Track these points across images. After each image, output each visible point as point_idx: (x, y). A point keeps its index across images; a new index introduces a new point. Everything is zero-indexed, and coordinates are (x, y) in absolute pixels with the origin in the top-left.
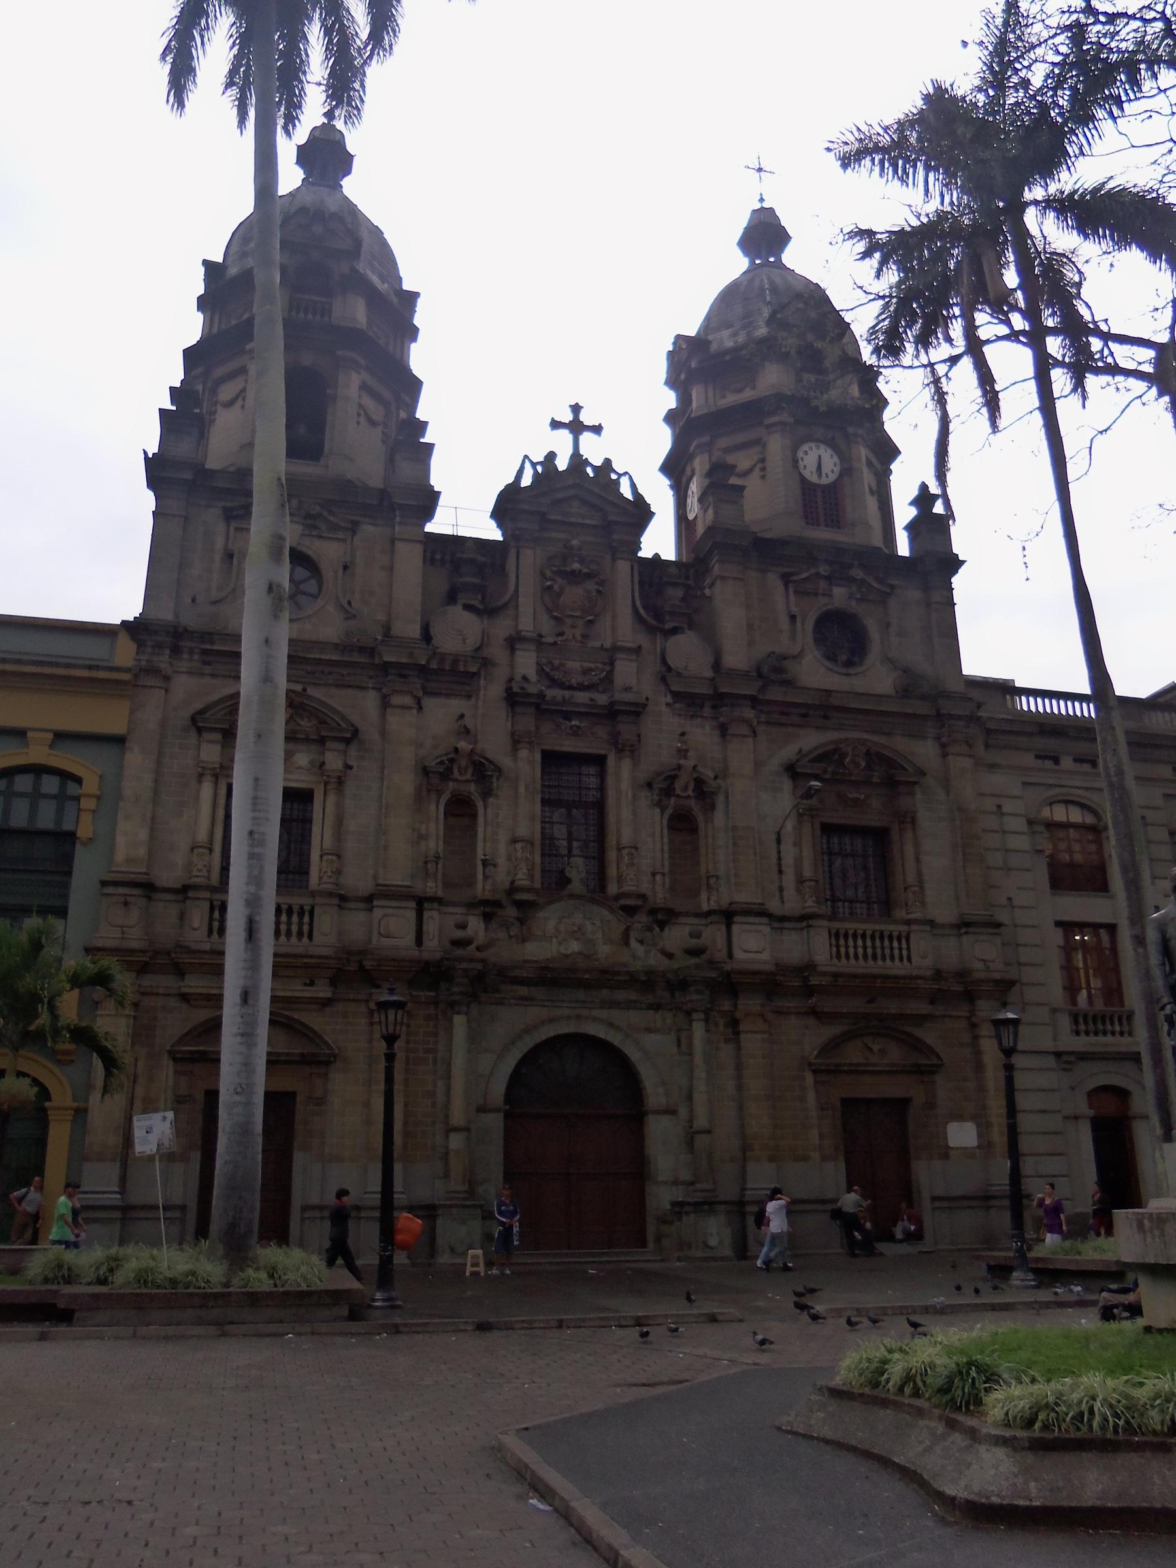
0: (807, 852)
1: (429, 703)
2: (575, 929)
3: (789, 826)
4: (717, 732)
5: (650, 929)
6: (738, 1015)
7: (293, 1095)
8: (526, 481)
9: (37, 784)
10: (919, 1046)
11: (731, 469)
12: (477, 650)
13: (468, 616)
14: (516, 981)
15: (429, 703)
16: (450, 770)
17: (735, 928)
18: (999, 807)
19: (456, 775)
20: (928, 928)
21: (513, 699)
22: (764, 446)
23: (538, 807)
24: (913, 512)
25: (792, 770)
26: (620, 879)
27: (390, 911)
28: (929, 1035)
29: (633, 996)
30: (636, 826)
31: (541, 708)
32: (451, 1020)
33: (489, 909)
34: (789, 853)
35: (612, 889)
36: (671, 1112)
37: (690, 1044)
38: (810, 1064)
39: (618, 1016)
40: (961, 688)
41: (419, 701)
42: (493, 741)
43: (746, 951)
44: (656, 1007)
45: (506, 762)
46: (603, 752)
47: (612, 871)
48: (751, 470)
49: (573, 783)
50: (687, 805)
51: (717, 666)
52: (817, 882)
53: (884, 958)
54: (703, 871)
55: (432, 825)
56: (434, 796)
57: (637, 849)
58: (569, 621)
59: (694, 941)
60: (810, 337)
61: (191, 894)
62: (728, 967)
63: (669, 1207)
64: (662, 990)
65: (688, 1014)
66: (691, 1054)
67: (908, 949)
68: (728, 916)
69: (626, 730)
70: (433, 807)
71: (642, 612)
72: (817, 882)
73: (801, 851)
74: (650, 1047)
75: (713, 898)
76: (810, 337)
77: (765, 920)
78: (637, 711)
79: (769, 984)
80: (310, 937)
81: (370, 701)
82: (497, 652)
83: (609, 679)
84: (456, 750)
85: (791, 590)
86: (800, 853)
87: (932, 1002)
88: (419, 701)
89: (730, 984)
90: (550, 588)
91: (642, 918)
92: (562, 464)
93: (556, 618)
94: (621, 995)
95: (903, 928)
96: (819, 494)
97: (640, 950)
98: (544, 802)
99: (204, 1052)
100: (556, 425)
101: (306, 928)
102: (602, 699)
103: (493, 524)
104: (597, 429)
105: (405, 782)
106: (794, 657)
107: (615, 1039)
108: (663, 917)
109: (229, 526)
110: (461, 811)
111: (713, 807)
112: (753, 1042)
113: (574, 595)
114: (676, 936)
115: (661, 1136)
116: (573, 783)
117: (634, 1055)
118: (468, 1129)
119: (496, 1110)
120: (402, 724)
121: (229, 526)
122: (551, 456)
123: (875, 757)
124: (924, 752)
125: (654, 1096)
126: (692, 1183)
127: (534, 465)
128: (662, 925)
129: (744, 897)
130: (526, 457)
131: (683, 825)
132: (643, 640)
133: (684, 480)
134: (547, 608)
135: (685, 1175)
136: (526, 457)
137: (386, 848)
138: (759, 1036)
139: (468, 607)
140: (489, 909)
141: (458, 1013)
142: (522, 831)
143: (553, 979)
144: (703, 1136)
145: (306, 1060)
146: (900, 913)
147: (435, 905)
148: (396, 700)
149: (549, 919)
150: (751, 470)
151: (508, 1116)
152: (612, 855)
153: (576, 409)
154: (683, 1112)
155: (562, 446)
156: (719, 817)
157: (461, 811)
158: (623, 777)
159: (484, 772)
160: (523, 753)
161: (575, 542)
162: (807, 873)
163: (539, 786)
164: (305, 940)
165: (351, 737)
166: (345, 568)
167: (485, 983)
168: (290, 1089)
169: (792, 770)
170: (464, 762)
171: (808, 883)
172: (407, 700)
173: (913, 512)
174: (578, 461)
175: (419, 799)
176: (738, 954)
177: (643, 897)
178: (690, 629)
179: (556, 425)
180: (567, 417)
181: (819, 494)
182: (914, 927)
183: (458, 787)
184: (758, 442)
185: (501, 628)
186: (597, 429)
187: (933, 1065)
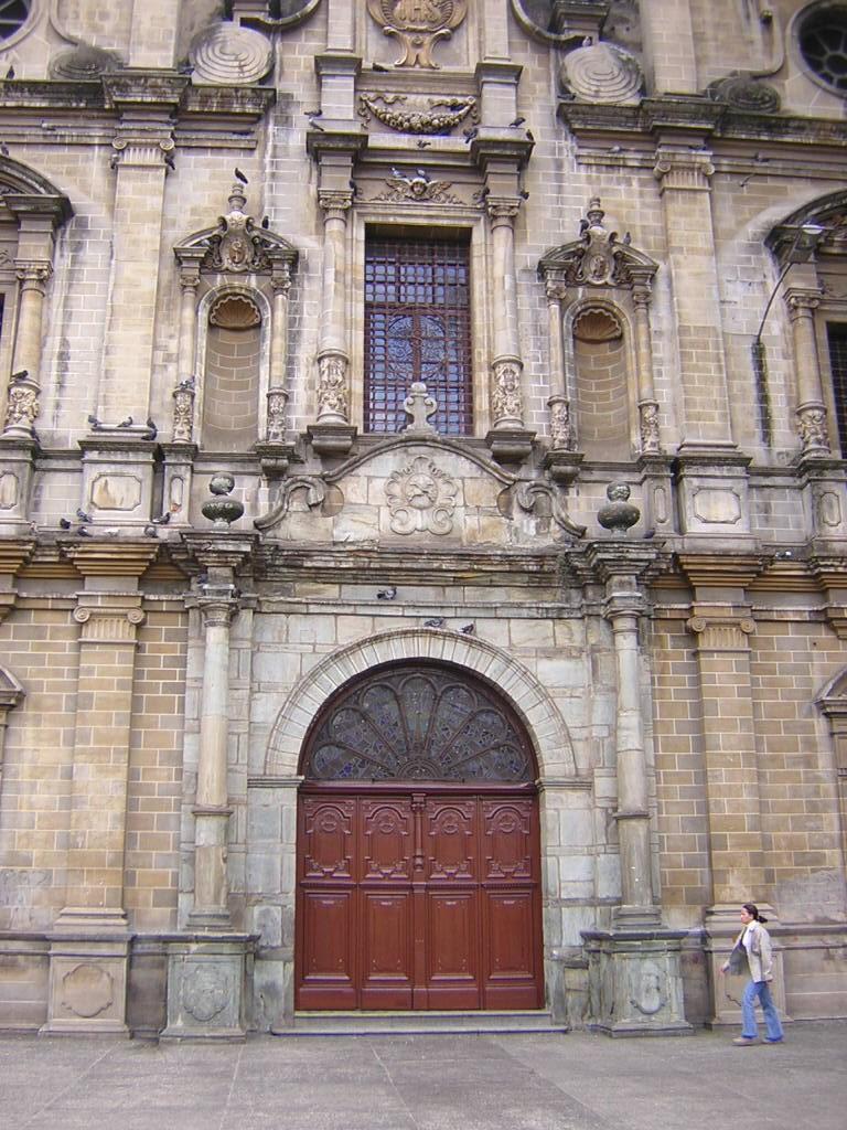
0: (808, 367)
1: (185, 160)
2: (418, 492)
3: (776, 327)
4: (651, 190)
9: (391, 283)
12: (262, 81)
13: (250, 34)
14: (319, 575)
15: (185, 160)
19: (227, 263)
21: (320, 147)
25: (778, 240)
26: (493, 415)
27: (105, 469)
29: (517, 596)
31: (360, 156)
32: (204, 638)
33: (274, 464)
35: (482, 429)
36: (582, 784)
37: (616, 674)
38: (821, 705)
39: (488, 630)
41: (169, 161)
42: (291, 219)
43: (705, 521)
44: (558, 616)
45: (307, 243)
46: (465, 223)
47: (482, 402)
49: (419, 262)
50: (600, 293)
52: (826, 411)
54: (633, 397)
55: (187, 339)
56: (190, 296)
57: (521, 366)
58: (424, 342)
59: (619, 502)
62: (674, 546)
63: (578, 941)
64: (572, 576)
65: (610, 622)
66: (615, 690)
68: (676, 467)
69: (501, 186)
70: (188, 313)
71: (525, 18)
72: (826, 411)
73: (796, 365)
74: (553, 673)
75: (650, 439)
77: (739, 471)
78: (519, 155)
79: (754, 573)
81: (94, 164)
82: (295, 83)
84: (223, 223)
88: (169, 161)
89: (675, 575)
91: (530, 473)
93: (391, 35)
97: (529, 525)
105: (143, 273)
106: (771, 75)
108: (565, 470)
110: (234, 318)
111: (647, 301)
112: (724, 674)
114: (583, 507)
115: (567, 823)
116: (419, 262)
117: (519, 694)
118: (197, 814)
120: (141, 190)
125: (553, 763)
126: (619, 901)
128: (564, 481)
131: (594, 329)
132: (526, 59)
134: (376, 23)
135: (606, 890)
137: (108, 374)
138: (733, 659)
139: (245, 23)
140: (274, 464)
141: (213, 624)
142: (332, 343)
143: (385, 570)
144: (633, 823)
148: (131, 157)
151: (304, 792)
152: (481, 378)
154: (602, 785)
156: (661, 317)
157: (234, 318)
158: (497, 264)
159: (275, 259)
160: (335, 226)
163: (361, 277)
165: (61, 213)
167: (265, 570)
169: (778, 240)
171: (810, 413)
172: (152, 157)
175: (162, 308)
176: (694, 527)
178: (601, 39)
183: (232, 279)
185: (300, 55)
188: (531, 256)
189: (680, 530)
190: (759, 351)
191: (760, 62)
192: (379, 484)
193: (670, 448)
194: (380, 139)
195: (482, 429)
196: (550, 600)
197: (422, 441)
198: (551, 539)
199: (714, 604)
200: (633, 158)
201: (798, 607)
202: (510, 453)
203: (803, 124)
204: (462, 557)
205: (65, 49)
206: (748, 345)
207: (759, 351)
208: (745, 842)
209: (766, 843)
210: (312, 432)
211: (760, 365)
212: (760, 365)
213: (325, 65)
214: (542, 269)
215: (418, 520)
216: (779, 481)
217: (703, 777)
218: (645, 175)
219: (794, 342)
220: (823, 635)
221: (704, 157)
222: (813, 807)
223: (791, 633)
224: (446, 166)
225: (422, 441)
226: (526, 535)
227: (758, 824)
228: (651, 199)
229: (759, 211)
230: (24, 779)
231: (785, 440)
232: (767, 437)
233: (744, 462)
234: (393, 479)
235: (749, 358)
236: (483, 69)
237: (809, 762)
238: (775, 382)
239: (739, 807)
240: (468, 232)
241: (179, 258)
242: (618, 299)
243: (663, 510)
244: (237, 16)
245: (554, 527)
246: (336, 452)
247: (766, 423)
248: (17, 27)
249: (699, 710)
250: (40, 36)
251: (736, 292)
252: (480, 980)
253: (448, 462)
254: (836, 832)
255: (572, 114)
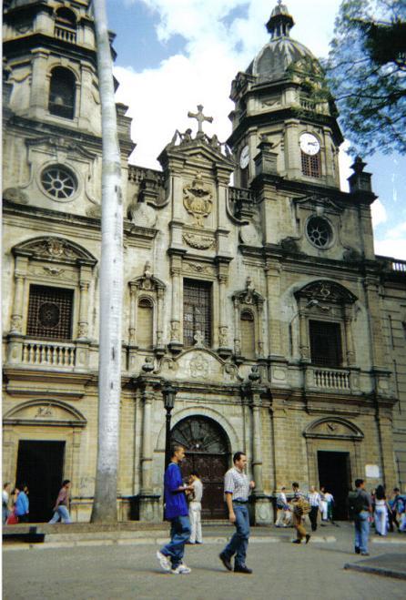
3: (296, 321)
4: (263, 274)
5: (233, 367)
6: (272, 409)
7: (63, 443)
8: (178, 142)
10: (354, 428)
11: (270, 144)
16: (244, 298)
17: (272, 368)
18: (390, 316)
19: (144, 287)
20: (87, 346)
22: (284, 135)
23: (182, 305)
24: (352, 172)
25: (298, 295)
28: (357, 422)
29: (225, 397)
30: (225, 314)
31: (182, 254)
34: (296, 333)
35: (216, 346)
39: (217, 408)
40: (374, 259)
42: (161, 271)
45: (167, 282)
47: (216, 338)
48: (24, 80)
50: (249, 304)
51: (264, 242)
53: (41, 361)
60: (308, 79)
61: (11, 339)
64: (244, 393)
67: (75, 358)
76: (308, 79)
77: (285, 365)
79: (288, 395)
80: (74, 363)
83: (216, 245)
84: (145, 275)
85: (298, 206)
86: (301, 335)
87: (86, 385)
90: (187, 198)
91: (229, 361)
92: (194, 136)
93: (190, 214)
94: (220, 397)
95: (347, 372)
96: (309, 159)
98: (185, 304)
99: (18, 421)
100: (190, 115)
101: (72, 359)
102: (211, 254)
103: (158, 163)
104: (210, 120)
106: (298, 239)
107: (217, 418)
108: (238, 361)
109: (28, 150)
113: (198, 202)
114: (245, 371)
116: (198, 289)
117: (225, 427)
119: (162, 451)
121: (28, 150)
122: (189, 132)
123: (69, 246)
124: (355, 287)
127: (180, 136)
128: (239, 364)
129: (276, 353)
130: (177, 131)
131: (247, 316)
133: (240, 148)
136: (177, 131)
139: (149, 204)
145: (71, 425)
146: (345, 365)
147: (135, 351)
149: (186, 360)
150: (24, 80)
152: (216, 331)
153: (200, 108)
155: (193, 125)
156: (264, 316)
157: (145, 304)
159: (156, 285)
160: (176, 279)
161: (199, 176)
162: (304, 343)
164: (72, 365)
166: (89, 178)
168: (345, 451)
169: (298, 295)
170: (249, 295)
173: (352, 172)
174: (201, 136)
176: (273, 381)
177: (230, 351)
179: (190, 115)
180: (195, 111)
181: (309, 159)
182: (78, 345)
184: (29, 64)
185: (165, 216)
186: (210, 120)
187: (80, 422)
188: (231, 293)
189: (270, 381)
190: (290, 327)
191: (296, 235)
192: (188, 362)
193: (266, 356)
194: (190, 251)
195: (216, 346)
196: (234, 399)
197: (200, 349)
198: (234, 381)
199: (277, 403)
200: (258, 262)
201: (299, 405)
202: (222, 355)
203: (306, 257)
204: (212, 386)
205: (91, 204)
206: (288, 325)
207: (290, 327)
208: (284, 473)
209: (289, 473)
210: (170, 346)
211: (291, 332)
212: (291, 332)
213: (171, 225)
214: (233, 298)
215: (199, 373)
216: (293, 367)
217: (274, 453)
218: (262, 269)
219: (300, 326)
220: (305, 414)
221: (279, 265)
222: (301, 463)
223: (296, 413)
224: (205, 260)
225: (200, 349)
226: (228, 380)
227: (287, 467)
228: (263, 277)
229: (292, 284)
230: (87, 449)
231: (296, 357)
232: (292, 354)
233: (286, 362)
234: (192, 360)
235: (287, 329)
236: (218, 231)
237: (300, 450)
238: (295, 337)
239: (283, 462)
240: (212, 283)
241: (130, 284)
242: (253, 308)
243: (265, 375)
244: (146, 201)
245: (235, 378)
246: (174, 351)
247: (292, 350)
248: (64, 197)
249: (273, 433)
250: (81, 197)
251: (286, 309)
252: (212, 511)
253: (206, 356)
254: (306, 470)
255: (243, 248)
